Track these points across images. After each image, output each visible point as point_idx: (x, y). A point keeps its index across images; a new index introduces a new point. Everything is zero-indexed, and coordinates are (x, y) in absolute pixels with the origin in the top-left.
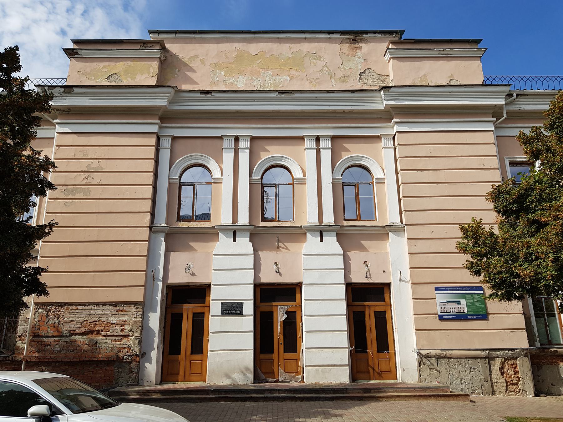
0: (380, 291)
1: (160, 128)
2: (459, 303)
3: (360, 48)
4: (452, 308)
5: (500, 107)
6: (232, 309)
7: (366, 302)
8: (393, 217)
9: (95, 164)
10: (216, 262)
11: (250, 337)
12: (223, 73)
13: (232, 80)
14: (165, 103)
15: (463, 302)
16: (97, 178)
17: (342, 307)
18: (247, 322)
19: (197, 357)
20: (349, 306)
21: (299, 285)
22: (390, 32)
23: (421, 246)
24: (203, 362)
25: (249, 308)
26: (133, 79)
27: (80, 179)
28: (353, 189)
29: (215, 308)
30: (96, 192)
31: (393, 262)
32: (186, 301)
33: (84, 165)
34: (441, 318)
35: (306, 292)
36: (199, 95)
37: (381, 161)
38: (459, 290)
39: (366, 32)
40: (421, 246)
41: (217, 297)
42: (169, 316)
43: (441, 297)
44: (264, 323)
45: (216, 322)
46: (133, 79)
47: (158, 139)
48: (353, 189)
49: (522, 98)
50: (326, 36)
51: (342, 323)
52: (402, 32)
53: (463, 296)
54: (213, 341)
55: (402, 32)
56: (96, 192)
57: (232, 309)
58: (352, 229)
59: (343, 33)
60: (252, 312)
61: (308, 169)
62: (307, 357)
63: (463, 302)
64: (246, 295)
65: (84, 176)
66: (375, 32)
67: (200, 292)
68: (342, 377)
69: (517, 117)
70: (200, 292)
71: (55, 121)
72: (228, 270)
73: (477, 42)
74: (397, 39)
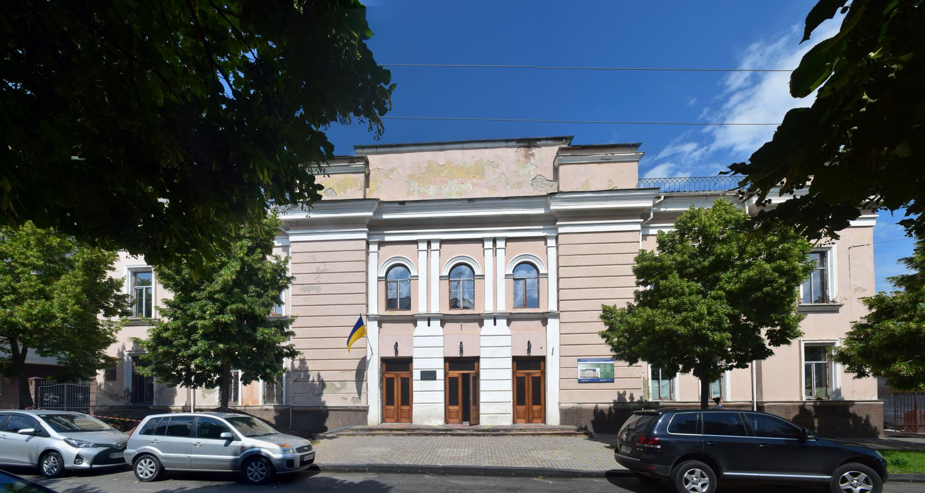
0: (539, 362)
1: (369, 235)
2: (594, 370)
3: (533, 155)
4: (590, 375)
5: (649, 209)
6: (429, 375)
7: (529, 372)
8: (553, 307)
9: (322, 267)
10: (417, 342)
11: (483, 397)
12: (416, 184)
13: (425, 190)
14: (371, 214)
15: (598, 370)
16: (324, 278)
17: (509, 374)
18: (439, 384)
19: (405, 408)
20: (514, 373)
21: (477, 359)
22: (560, 139)
23: (570, 328)
24: (410, 411)
25: (440, 375)
26: (345, 192)
27: (311, 279)
28: (460, 275)
29: (416, 375)
30: (325, 289)
31: (550, 341)
32: (397, 368)
33: (313, 268)
34: (580, 381)
35: (483, 363)
36: (398, 205)
37: (547, 259)
38: (597, 360)
39: (540, 140)
40: (570, 328)
41: (418, 366)
42: (385, 380)
43: (581, 366)
44: (451, 384)
45: (418, 385)
46: (345, 192)
47: (368, 244)
48: (460, 275)
49: (668, 200)
50: (504, 144)
51: (509, 385)
52: (571, 138)
53: (599, 366)
54: (417, 398)
55: (571, 138)
56: (325, 289)
57: (429, 375)
58: (460, 311)
59: (519, 141)
60: (443, 378)
61: (494, 268)
62: (417, 409)
63: (598, 370)
64: (438, 366)
65: (314, 276)
66: (547, 139)
67: (406, 363)
68: (438, 422)
69: (661, 217)
70: (406, 363)
71: (289, 232)
72: (428, 347)
73: (635, 146)
74: (566, 146)
